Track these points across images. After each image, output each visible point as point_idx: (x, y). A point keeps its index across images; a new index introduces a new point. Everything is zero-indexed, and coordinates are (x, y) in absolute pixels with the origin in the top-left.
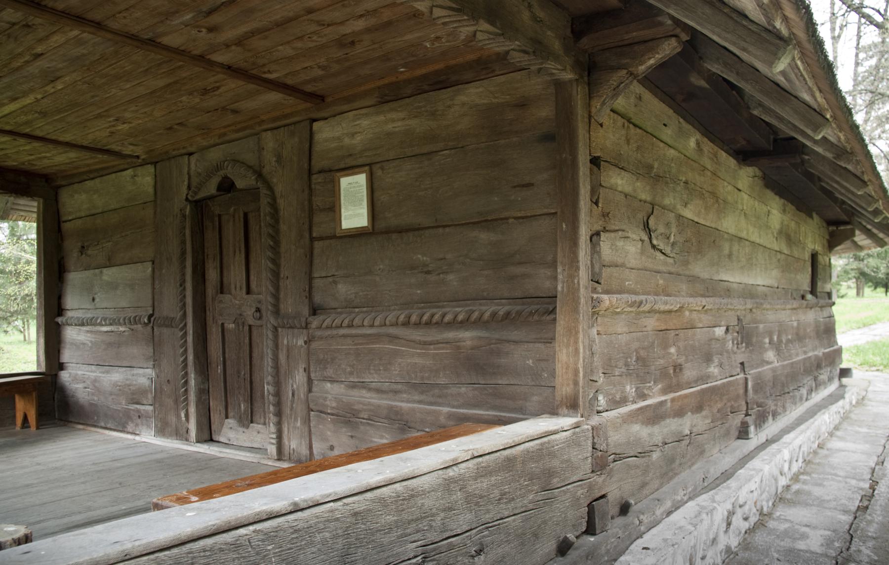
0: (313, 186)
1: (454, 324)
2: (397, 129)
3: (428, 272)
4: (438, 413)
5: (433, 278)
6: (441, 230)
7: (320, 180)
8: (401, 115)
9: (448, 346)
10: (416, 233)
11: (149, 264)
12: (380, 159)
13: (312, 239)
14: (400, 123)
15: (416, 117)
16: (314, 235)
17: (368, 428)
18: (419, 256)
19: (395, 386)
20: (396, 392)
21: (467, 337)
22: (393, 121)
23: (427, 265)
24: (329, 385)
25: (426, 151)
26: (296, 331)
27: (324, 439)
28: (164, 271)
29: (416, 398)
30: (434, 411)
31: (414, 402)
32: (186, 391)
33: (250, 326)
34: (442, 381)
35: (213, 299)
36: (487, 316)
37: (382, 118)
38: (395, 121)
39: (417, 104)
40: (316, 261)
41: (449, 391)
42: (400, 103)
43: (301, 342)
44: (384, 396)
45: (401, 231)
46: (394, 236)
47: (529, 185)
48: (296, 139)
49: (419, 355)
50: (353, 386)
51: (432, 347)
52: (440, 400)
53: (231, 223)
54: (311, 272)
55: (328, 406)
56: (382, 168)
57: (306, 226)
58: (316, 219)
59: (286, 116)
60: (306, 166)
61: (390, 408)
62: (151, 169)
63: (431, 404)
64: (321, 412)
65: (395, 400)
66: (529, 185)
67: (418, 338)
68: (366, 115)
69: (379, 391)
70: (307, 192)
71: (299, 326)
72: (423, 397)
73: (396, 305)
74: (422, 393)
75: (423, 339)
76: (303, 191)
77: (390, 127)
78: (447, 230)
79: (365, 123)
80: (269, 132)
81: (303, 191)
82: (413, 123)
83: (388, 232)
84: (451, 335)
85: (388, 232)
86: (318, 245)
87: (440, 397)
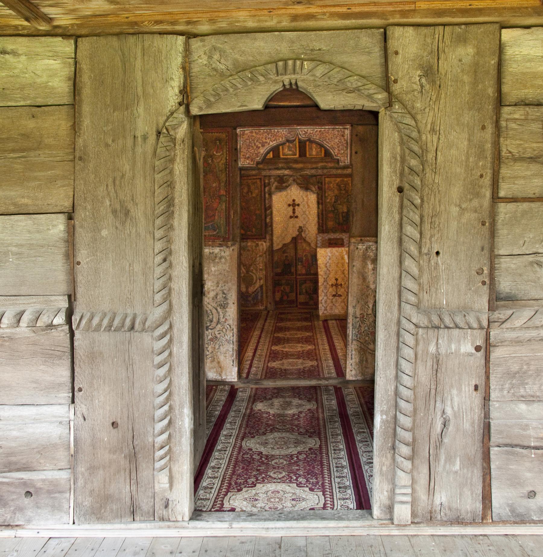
0: (503, 124)
7: (516, 116)
11: (62, 218)
13: (495, 198)
16: (502, 194)
24: (523, 407)
26: (456, 332)
27: (515, 481)
28: (104, 233)
40: (502, 231)
48: (471, 50)
54: (492, 249)
55: (530, 437)
57: (487, 180)
58: (504, 171)
59: (480, 11)
60: (491, 91)
62: (66, 47)
64: (512, 446)
70: (490, 129)
71: (475, 325)
76: (483, 128)
81: (483, 128)
86: (503, 209)
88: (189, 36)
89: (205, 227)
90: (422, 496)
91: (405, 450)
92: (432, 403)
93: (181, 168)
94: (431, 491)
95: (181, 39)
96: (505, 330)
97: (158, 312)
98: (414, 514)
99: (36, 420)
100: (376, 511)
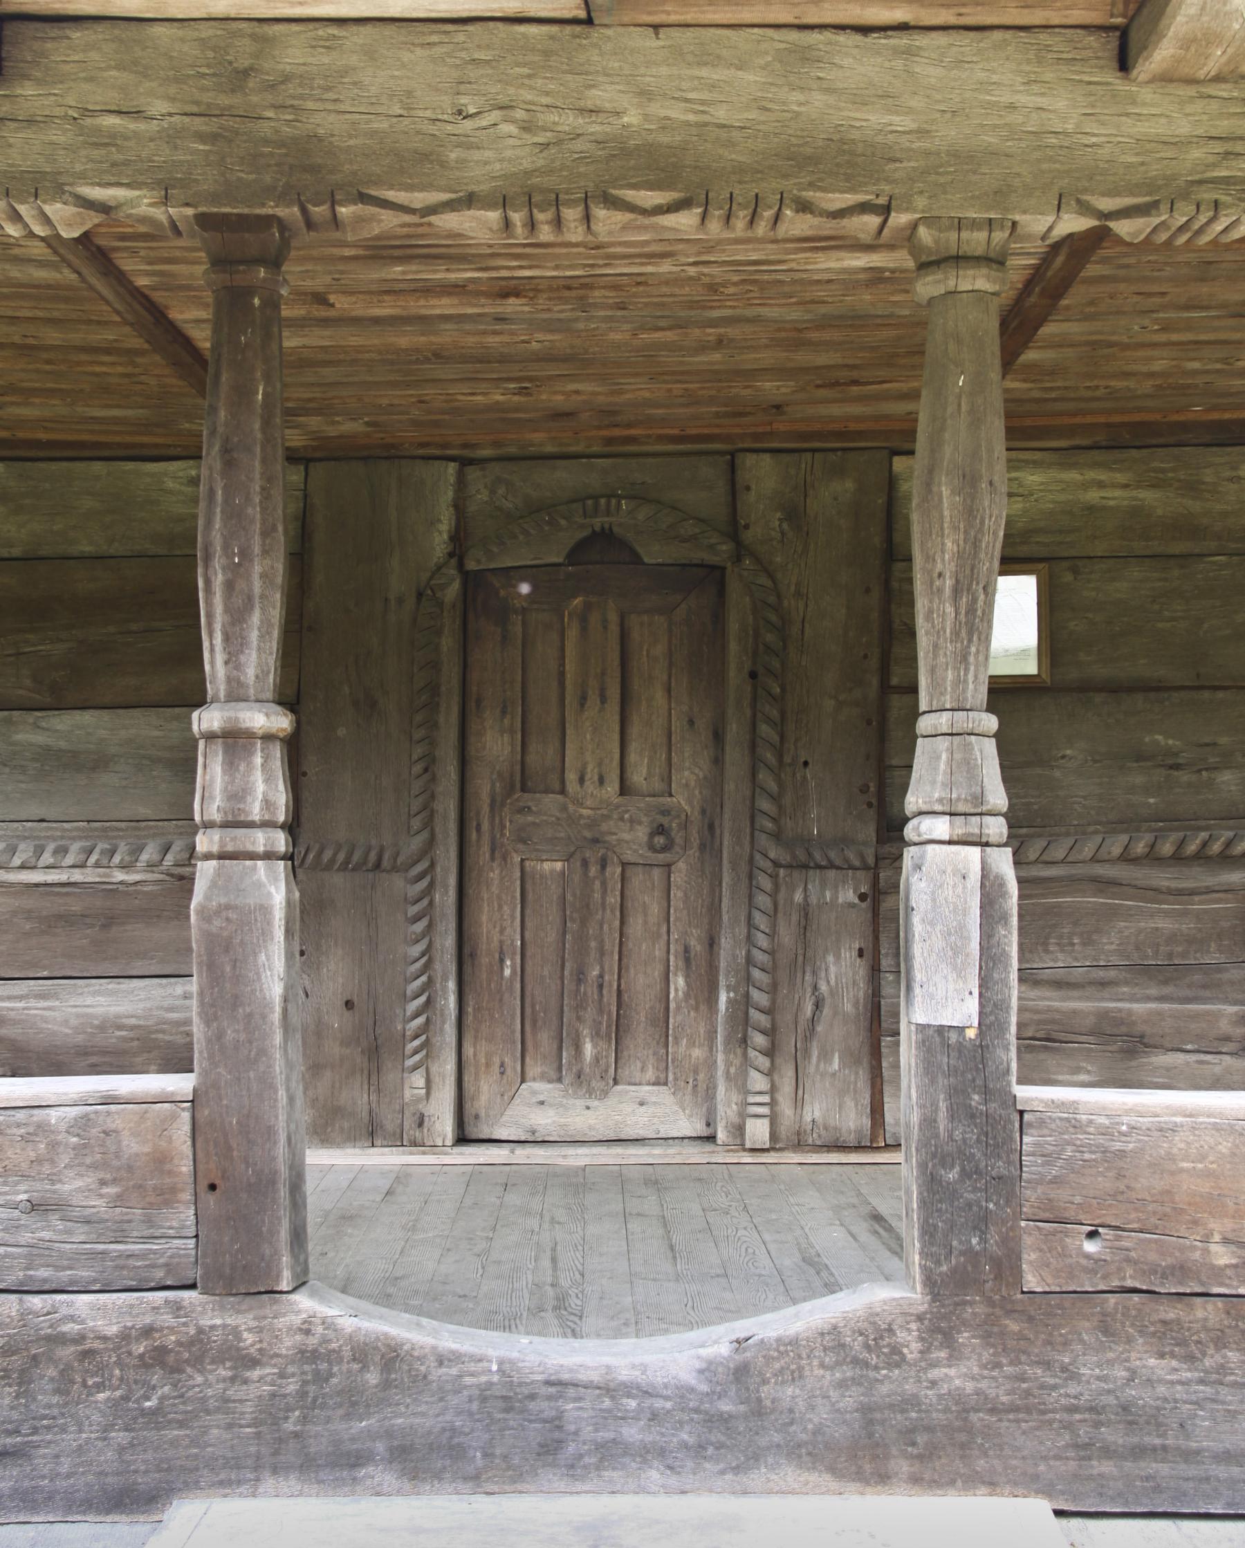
2: (1111, 503)
3: (1177, 767)
4: (1217, 1016)
5: (1184, 777)
6: (1206, 695)
8: (1120, 478)
9: (1230, 896)
10: (1152, 695)
12: (1073, 553)
14: (1118, 493)
15: (1153, 486)
16: (895, 681)
17: (1042, 1056)
18: (1159, 737)
19: (1101, 973)
20: (1103, 984)
22: (1101, 485)
23: (1176, 754)
25: (1177, 552)
26: (832, 874)
29: (1153, 991)
30: (1208, 1013)
31: (1149, 999)
33: (624, 865)
34: (1213, 957)
35: (495, 805)
37: (1073, 475)
39: (1155, 464)
41: (1225, 976)
42: (1117, 454)
43: (848, 895)
44: (1075, 993)
45: (1115, 689)
46: (1098, 698)
48: (849, 485)
49: (1167, 913)
51: (1196, 898)
52: (1207, 993)
56: (1075, 571)
57: (874, 663)
61: (1103, 1015)
63: (1188, 1000)
65: (1103, 999)
67: (1166, 883)
68: (1036, 464)
69: (1058, 984)
72: (1168, 990)
73: (1100, 823)
74: (1166, 982)
75: (1174, 884)
76: (868, 590)
77: (1093, 496)
78: (1220, 695)
80: (767, 457)
81: (868, 590)
82: (1148, 496)
83: (1085, 688)
85: (1085, 688)
87: (1204, 987)
90: (786, 1109)
91: (759, 1040)
95: (452, 468)
97: (417, 843)
98: (774, 1136)
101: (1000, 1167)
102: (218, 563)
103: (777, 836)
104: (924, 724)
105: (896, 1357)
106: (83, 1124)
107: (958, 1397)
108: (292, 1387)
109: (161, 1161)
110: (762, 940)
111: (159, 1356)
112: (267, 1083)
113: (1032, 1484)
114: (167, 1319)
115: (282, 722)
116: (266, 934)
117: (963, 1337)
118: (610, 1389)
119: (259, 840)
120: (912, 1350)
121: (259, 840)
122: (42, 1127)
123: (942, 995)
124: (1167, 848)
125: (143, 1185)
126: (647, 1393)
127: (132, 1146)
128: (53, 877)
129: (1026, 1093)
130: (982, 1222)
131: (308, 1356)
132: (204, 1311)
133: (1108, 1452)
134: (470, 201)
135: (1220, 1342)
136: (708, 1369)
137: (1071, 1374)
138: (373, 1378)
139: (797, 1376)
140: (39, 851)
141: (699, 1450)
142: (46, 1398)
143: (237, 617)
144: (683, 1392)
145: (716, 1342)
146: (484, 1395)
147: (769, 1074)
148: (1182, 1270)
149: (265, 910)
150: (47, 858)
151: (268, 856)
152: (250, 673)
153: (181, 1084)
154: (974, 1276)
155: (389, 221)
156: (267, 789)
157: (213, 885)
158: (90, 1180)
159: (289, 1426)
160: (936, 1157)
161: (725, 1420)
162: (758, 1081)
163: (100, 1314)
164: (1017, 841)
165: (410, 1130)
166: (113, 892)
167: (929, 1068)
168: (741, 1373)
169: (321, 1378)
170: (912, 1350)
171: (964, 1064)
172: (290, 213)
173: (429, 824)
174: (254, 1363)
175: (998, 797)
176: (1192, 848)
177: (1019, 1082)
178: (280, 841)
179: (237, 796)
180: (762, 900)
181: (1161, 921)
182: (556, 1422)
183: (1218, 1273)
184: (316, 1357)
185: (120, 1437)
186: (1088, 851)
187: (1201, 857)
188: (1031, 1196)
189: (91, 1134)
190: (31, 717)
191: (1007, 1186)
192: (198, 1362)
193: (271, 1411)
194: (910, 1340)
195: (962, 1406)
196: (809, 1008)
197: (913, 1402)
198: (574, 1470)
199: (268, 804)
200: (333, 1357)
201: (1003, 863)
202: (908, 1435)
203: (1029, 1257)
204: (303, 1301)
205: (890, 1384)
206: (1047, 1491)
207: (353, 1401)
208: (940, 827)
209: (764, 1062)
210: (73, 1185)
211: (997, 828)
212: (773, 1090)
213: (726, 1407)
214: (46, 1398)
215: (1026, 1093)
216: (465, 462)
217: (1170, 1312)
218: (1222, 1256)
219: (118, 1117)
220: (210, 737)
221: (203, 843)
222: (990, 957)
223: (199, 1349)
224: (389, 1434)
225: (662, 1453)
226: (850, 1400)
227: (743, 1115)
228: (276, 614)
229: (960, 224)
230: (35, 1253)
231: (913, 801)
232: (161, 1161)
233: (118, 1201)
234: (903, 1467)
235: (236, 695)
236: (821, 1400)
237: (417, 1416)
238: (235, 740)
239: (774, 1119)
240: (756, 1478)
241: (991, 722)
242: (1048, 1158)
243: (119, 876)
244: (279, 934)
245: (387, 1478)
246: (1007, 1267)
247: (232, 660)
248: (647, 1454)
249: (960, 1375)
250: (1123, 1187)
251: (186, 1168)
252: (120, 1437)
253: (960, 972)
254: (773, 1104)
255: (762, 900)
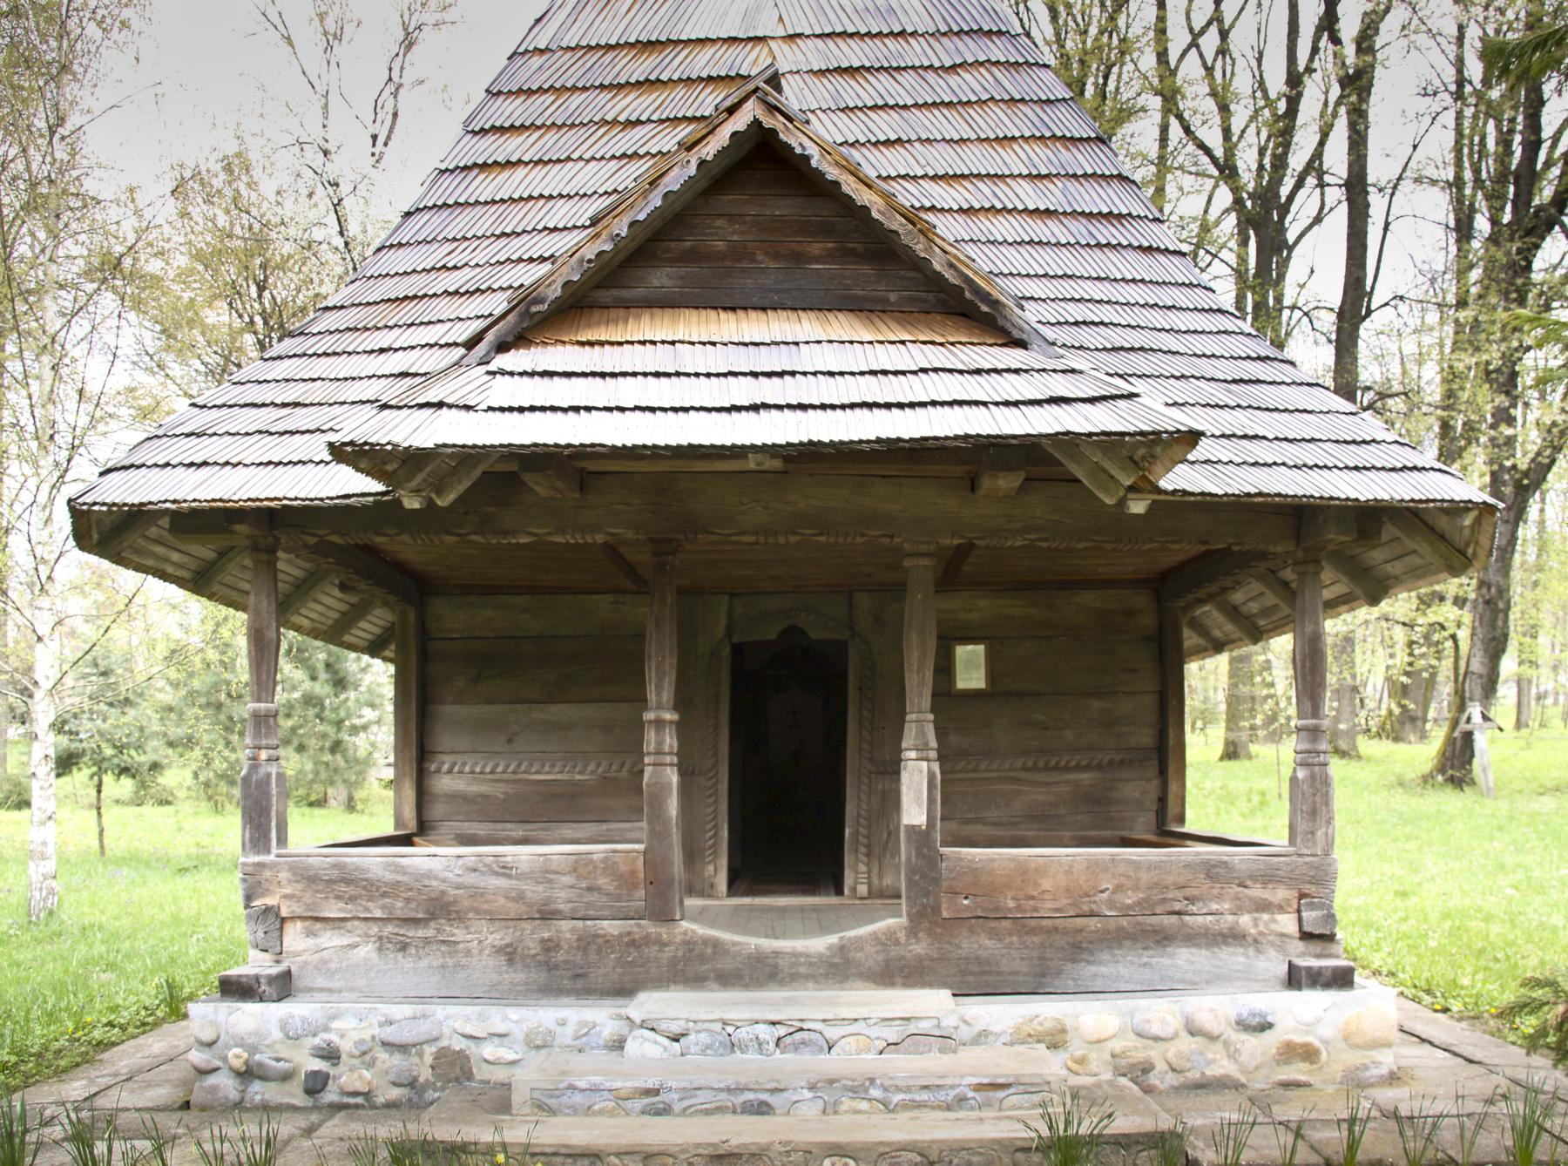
1: (1078, 768)
20: (1014, 824)
21: (1086, 777)
32: (715, 826)
34: (1062, 811)
36: (1105, 762)
38: (1014, 607)
45: (1020, 695)
47: (1134, 670)
50: (968, 821)
53: (1187, 918)
66: (1134, 670)
69: (995, 824)
79: (982, 603)
84: (1070, 776)
88: (732, 595)
89: (899, 897)
90: (875, 880)
91: (863, 849)
92: (1045, 923)
93: (725, 675)
94: (880, 877)
95: (726, 598)
96: (66, 667)
97: (710, 763)
98: (870, 892)
99: (631, 830)
100: (846, 892)
101: (934, 874)
102: (653, 660)
103: (871, 760)
104: (908, 717)
105: (897, 942)
106: (605, 860)
107: (919, 956)
108: (680, 954)
109: (633, 873)
110: (864, 806)
111: (633, 943)
112: (671, 845)
113: (944, 985)
114: (636, 929)
115: (675, 717)
116: (670, 793)
117: (921, 935)
118: (795, 955)
119: (668, 759)
120: (903, 939)
121: (668, 759)
122: (591, 861)
123: (914, 811)
124: (1041, 764)
125: (627, 882)
126: (807, 956)
127: (623, 868)
128: (549, 777)
129: (943, 850)
130: (927, 894)
131: (686, 943)
132: (649, 927)
133: (971, 973)
134: (744, 533)
135: (1011, 934)
136: (830, 948)
137: (959, 947)
138: (709, 951)
139: (862, 949)
140: (543, 766)
141: (827, 976)
142: (593, 957)
143: (660, 679)
144: (821, 955)
145: (833, 939)
146: (749, 956)
147: (867, 864)
148: (997, 909)
149: (670, 784)
150: (547, 769)
151: (671, 765)
152: (665, 699)
153: (641, 847)
154: (925, 917)
155: (715, 538)
156: (670, 741)
157: (651, 775)
158: (607, 880)
159: (680, 967)
160: (912, 871)
161: (835, 965)
162: (862, 868)
163: (610, 927)
164: (941, 758)
165: (707, 890)
166: (575, 784)
167: (909, 839)
168: (842, 949)
169: (691, 951)
170: (903, 939)
171: (921, 837)
172: (681, 537)
173: (715, 754)
174: (666, 945)
175: (934, 743)
176: (1052, 763)
177: (945, 844)
178: (675, 760)
179: (660, 743)
180: (864, 788)
181: (1038, 796)
182: (775, 966)
183: (1010, 910)
184: (689, 944)
185: (619, 970)
186: (1007, 766)
187: (1057, 768)
188: (945, 884)
189: (609, 866)
190: (539, 706)
191: (936, 881)
192: (647, 945)
193: (673, 962)
194: (902, 936)
195: (920, 958)
196: (885, 836)
197: (903, 958)
198: (783, 983)
199: (671, 746)
200: (695, 943)
201: (936, 767)
202: (901, 969)
203: (944, 906)
204: (684, 924)
205: (895, 952)
206: (950, 987)
207: (703, 959)
208: (913, 754)
209: (865, 859)
210: (602, 882)
211: (933, 754)
212: (869, 872)
213: (836, 960)
214: (593, 957)
215: (943, 850)
216: (732, 595)
217: (993, 924)
218: (1011, 904)
219: (618, 858)
220: (650, 722)
221: (646, 760)
222: (931, 800)
223: (647, 940)
224: (715, 970)
225: (813, 977)
226: (880, 958)
227: (856, 883)
228: (674, 678)
229: (918, 542)
230: (589, 905)
231: (904, 745)
232: (633, 873)
233: (617, 888)
234: (900, 980)
235: (659, 707)
236: (870, 958)
237: (725, 964)
238: (659, 724)
239: (870, 885)
240: (847, 985)
241: (931, 717)
242: (951, 871)
243: (578, 777)
244: (675, 792)
245: (716, 986)
246: (936, 909)
247: (658, 694)
248: (807, 977)
249: (919, 948)
250: (981, 884)
251: (642, 876)
252: (619, 970)
253: (920, 805)
254: (869, 878)
255: (864, 788)
